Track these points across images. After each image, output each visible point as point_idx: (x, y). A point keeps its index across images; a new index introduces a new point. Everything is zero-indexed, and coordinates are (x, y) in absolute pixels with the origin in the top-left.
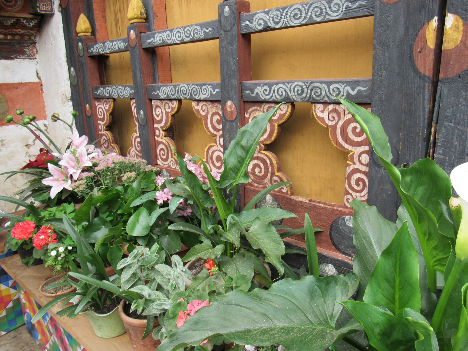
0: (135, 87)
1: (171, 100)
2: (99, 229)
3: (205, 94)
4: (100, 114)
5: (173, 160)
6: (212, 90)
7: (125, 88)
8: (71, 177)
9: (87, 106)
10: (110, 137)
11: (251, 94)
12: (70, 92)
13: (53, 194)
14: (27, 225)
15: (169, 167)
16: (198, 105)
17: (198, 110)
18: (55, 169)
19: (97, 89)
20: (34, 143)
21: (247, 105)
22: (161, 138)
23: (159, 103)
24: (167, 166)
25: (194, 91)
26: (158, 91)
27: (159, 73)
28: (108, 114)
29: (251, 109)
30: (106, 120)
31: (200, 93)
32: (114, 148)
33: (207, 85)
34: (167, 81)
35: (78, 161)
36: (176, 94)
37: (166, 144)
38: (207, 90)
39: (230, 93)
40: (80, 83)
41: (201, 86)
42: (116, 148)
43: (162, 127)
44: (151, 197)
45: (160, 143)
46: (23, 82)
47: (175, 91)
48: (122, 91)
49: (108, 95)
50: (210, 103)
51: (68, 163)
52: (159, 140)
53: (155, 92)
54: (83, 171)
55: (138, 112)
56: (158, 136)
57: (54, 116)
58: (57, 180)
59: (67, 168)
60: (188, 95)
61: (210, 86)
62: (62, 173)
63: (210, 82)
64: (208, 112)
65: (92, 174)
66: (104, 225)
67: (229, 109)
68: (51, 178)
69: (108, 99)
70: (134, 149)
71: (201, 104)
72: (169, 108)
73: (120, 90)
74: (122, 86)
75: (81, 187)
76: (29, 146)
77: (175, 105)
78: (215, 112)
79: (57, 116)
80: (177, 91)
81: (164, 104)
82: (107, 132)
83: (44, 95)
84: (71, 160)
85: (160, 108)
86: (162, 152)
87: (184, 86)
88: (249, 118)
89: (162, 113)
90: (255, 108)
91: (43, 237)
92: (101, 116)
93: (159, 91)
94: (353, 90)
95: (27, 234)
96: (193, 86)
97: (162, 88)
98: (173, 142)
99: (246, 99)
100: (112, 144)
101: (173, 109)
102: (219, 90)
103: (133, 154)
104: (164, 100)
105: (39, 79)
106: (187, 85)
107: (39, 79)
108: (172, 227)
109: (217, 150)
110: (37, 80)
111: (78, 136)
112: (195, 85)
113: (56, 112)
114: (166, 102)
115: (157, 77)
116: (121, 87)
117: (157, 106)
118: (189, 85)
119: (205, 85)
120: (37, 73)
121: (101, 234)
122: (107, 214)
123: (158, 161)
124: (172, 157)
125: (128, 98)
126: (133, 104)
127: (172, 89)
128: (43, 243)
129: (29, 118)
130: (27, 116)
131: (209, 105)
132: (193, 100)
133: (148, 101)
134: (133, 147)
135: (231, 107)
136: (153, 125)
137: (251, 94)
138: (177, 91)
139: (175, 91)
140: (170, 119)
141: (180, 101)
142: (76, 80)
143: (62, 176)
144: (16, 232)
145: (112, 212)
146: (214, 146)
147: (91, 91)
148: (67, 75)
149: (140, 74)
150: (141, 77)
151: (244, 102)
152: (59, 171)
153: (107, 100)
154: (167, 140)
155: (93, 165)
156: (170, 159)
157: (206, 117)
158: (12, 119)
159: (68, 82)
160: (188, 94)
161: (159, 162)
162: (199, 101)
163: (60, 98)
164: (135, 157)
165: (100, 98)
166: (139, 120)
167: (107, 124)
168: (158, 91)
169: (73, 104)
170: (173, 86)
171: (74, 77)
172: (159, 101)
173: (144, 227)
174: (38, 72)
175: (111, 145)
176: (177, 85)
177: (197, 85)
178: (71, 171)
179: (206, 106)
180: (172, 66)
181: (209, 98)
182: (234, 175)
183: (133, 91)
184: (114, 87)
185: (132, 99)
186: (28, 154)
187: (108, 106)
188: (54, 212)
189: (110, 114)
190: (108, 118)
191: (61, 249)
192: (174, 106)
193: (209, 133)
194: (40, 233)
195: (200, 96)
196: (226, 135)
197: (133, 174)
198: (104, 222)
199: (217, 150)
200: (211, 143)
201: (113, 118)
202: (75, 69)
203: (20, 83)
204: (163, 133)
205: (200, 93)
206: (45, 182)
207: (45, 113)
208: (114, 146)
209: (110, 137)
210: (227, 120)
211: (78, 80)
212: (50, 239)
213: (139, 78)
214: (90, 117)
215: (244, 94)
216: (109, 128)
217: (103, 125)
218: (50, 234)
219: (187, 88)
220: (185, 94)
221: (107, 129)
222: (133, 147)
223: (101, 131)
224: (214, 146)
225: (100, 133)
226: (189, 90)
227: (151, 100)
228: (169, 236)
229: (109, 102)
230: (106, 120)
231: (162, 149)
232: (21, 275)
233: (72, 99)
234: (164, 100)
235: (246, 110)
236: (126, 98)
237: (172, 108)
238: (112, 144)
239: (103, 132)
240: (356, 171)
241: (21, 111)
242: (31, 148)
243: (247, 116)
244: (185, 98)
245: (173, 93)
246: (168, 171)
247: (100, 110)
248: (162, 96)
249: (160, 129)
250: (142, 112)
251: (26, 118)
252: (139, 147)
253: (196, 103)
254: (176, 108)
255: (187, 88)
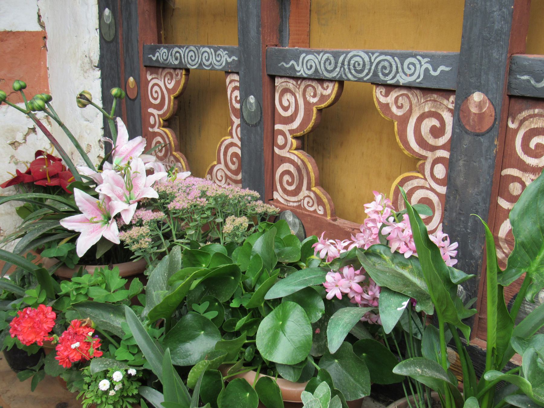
0: (244, 49)
1: (321, 81)
2: (192, 337)
3: (411, 75)
4: (155, 95)
5: (312, 195)
6: (430, 68)
7: (215, 52)
8: (118, 217)
9: (131, 79)
10: (171, 139)
11: (533, 82)
12: (99, 53)
13: (82, 247)
14: (41, 316)
15: (299, 207)
16: (386, 95)
17: (388, 104)
18: (88, 200)
19: (153, 50)
20: (25, 139)
21: (516, 105)
22: (288, 150)
23: (291, 85)
24: (295, 204)
25: (384, 67)
26: (292, 62)
27: (292, 27)
28: (172, 98)
29: (525, 114)
30: (166, 107)
31: (397, 72)
32: (178, 160)
33: (419, 57)
34: (303, 42)
35: (130, 186)
36: (338, 69)
37: (299, 163)
38: (418, 66)
39: (484, 77)
40: (120, 36)
41: (403, 57)
42: (182, 160)
43: (291, 131)
44: (310, 281)
45: (283, 160)
46: (14, 30)
47: (202, 58)
48: (210, 57)
49: (177, 62)
50: (418, 92)
51: (113, 191)
52: (283, 155)
53: (233, 60)
54: (138, 208)
55: (243, 100)
56: (282, 148)
57: (81, 96)
58: (86, 221)
59: (109, 199)
60: (367, 74)
61: (426, 60)
62: (98, 207)
63: (422, 52)
64: (410, 111)
65: (161, 215)
66: (203, 330)
67: (474, 110)
68: (77, 217)
69: (175, 69)
70: (222, 166)
71: (394, 94)
72: (315, 96)
73: (206, 54)
74: (210, 47)
75: (141, 239)
76: (16, 144)
77: (331, 90)
78: (430, 112)
79: (87, 96)
80: (339, 65)
81: (302, 87)
82: (167, 130)
83: (48, 54)
84: (117, 183)
85: (293, 94)
86: (286, 178)
87: (358, 56)
88: (516, 131)
89: (295, 106)
90: (536, 111)
91: (77, 344)
92: (155, 99)
93: (297, 61)
94: (435, 70)
95: (42, 333)
96: (383, 57)
97: (303, 55)
98: (313, 160)
99: (516, 93)
100: (174, 153)
101: (323, 98)
102: (236, 59)
103: (219, 174)
104: (304, 79)
105: (42, 25)
106: (367, 53)
107: (42, 25)
108: (400, 368)
109: (422, 187)
110: (37, 28)
111: (128, 137)
112: (386, 54)
113: (87, 90)
114: (310, 83)
115: (286, 34)
116: (207, 49)
117: (286, 91)
118: (373, 54)
119: (414, 56)
120: (39, 16)
121: (200, 348)
122: (206, 304)
123: (275, 193)
124: (309, 188)
125: (221, 70)
126: (233, 82)
127: (328, 59)
128: (76, 357)
129: (42, 99)
130: (39, 96)
131: (415, 98)
132: (377, 85)
133: (267, 79)
134: (219, 162)
135: (480, 105)
136: (274, 124)
137: (533, 82)
138: (339, 65)
139: (336, 63)
140: (314, 118)
141: (341, 83)
142: (113, 32)
143: (99, 213)
144: (19, 329)
145: (217, 301)
146: (417, 178)
147: (141, 54)
148: (94, 22)
149: (258, 28)
150: (258, 33)
151: (511, 97)
152: (92, 203)
153: (172, 71)
154: (302, 157)
155: (161, 197)
156: (304, 192)
157: (404, 120)
158: (6, 97)
159: (96, 36)
160: (366, 71)
161: (276, 196)
162: (390, 87)
163: (80, 62)
164: (224, 181)
165: (159, 68)
166: (245, 114)
167: (168, 115)
168: (292, 62)
169: (102, 74)
170: (331, 53)
171: (109, 26)
172: (291, 81)
173: (298, 345)
174: (41, 15)
175: (172, 154)
176: (343, 53)
177: (393, 55)
178: (119, 206)
179: (408, 97)
180: (314, 16)
181: (420, 83)
182: (527, 257)
183: (234, 58)
184: (192, 48)
185: (228, 73)
186: (14, 159)
187: (173, 82)
188: (86, 286)
189: (175, 98)
190: (172, 104)
191: (118, 376)
192: (327, 92)
193: (406, 152)
194: (69, 334)
195: (398, 77)
196: (458, 160)
197: (244, 221)
198: (204, 324)
199: (422, 187)
200: (409, 171)
201: (180, 102)
202: (113, 12)
203: (8, 32)
204: (295, 142)
205: (397, 72)
206: (68, 223)
207: (48, 88)
208: (178, 156)
209: (171, 139)
210: (467, 132)
211: (116, 31)
212: (91, 350)
213: (253, 33)
214: (134, 100)
215: (513, 81)
216: (168, 123)
217: (159, 116)
218: (89, 340)
219: (367, 59)
220: (361, 71)
221: (166, 123)
222: (219, 162)
223: (153, 126)
224: (417, 178)
225: (150, 130)
226: (371, 63)
227: (273, 78)
228: (340, 363)
229: (177, 75)
230: (166, 107)
231: (288, 172)
232: (9, 394)
233: (101, 66)
234: (304, 79)
235: (511, 114)
236: (217, 70)
237: (322, 95)
238: (174, 153)
239: (156, 129)
240: (232, 144)
241: (22, 84)
242: (20, 148)
243: (511, 125)
244: (360, 80)
245: (329, 68)
246: (296, 214)
247: (156, 88)
248: (302, 70)
249: (287, 134)
250: (252, 99)
251: (37, 98)
252: (233, 163)
253: (383, 90)
254: (333, 96)
255: (367, 59)
